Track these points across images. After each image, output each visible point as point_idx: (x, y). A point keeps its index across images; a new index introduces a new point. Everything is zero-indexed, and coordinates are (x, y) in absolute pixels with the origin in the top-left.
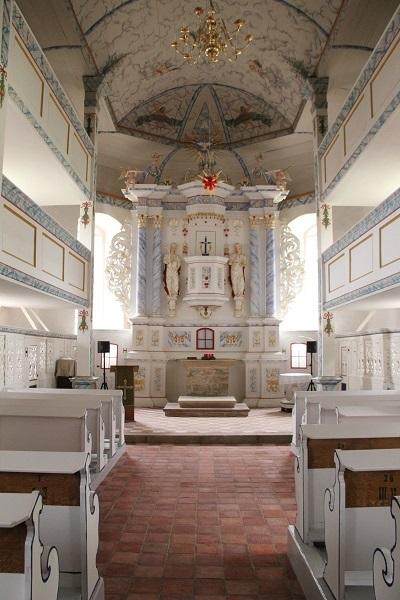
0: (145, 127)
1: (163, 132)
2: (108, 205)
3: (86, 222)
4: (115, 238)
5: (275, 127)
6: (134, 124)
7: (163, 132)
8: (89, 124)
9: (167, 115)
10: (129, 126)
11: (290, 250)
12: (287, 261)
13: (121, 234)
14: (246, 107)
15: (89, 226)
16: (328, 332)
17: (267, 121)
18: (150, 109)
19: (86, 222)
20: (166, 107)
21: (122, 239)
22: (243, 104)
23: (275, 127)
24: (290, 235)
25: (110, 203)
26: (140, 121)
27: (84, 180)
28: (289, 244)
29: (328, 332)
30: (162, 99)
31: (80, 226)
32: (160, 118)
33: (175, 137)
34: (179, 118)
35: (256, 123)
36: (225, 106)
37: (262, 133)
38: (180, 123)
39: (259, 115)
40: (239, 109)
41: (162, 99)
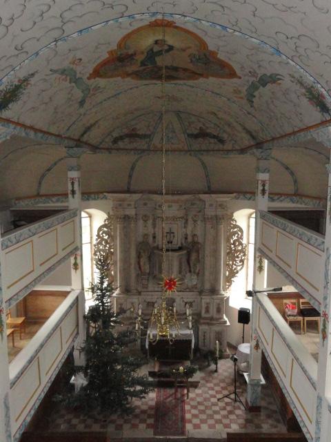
0: (121, 144)
1: (135, 145)
2: (94, 201)
3: (76, 269)
4: (100, 229)
5: (228, 146)
6: (111, 144)
7: (135, 145)
8: (7, 412)
9: (138, 132)
10: (106, 146)
11: (235, 238)
12: (232, 246)
13: (104, 226)
14: (204, 127)
15: (79, 271)
16: (257, 349)
17: (222, 141)
18: (124, 131)
19: (76, 269)
20: (138, 127)
21: (105, 229)
22: (201, 125)
23: (228, 146)
24: (236, 226)
25: (95, 199)
26: (115, 141)
27: (61, 247)
28: (235, 233)
29: (257, 349)
30: (133, 122)
31: (73, 271)
32: (133, 135)
33: (145, 147)
34: (149, 133)
35: (212, 140)
36: (186, 123)
37: (216, 148)
38: (149, 136)
39: (214, 136)
40: (198, 128)
41: (133, 122)
